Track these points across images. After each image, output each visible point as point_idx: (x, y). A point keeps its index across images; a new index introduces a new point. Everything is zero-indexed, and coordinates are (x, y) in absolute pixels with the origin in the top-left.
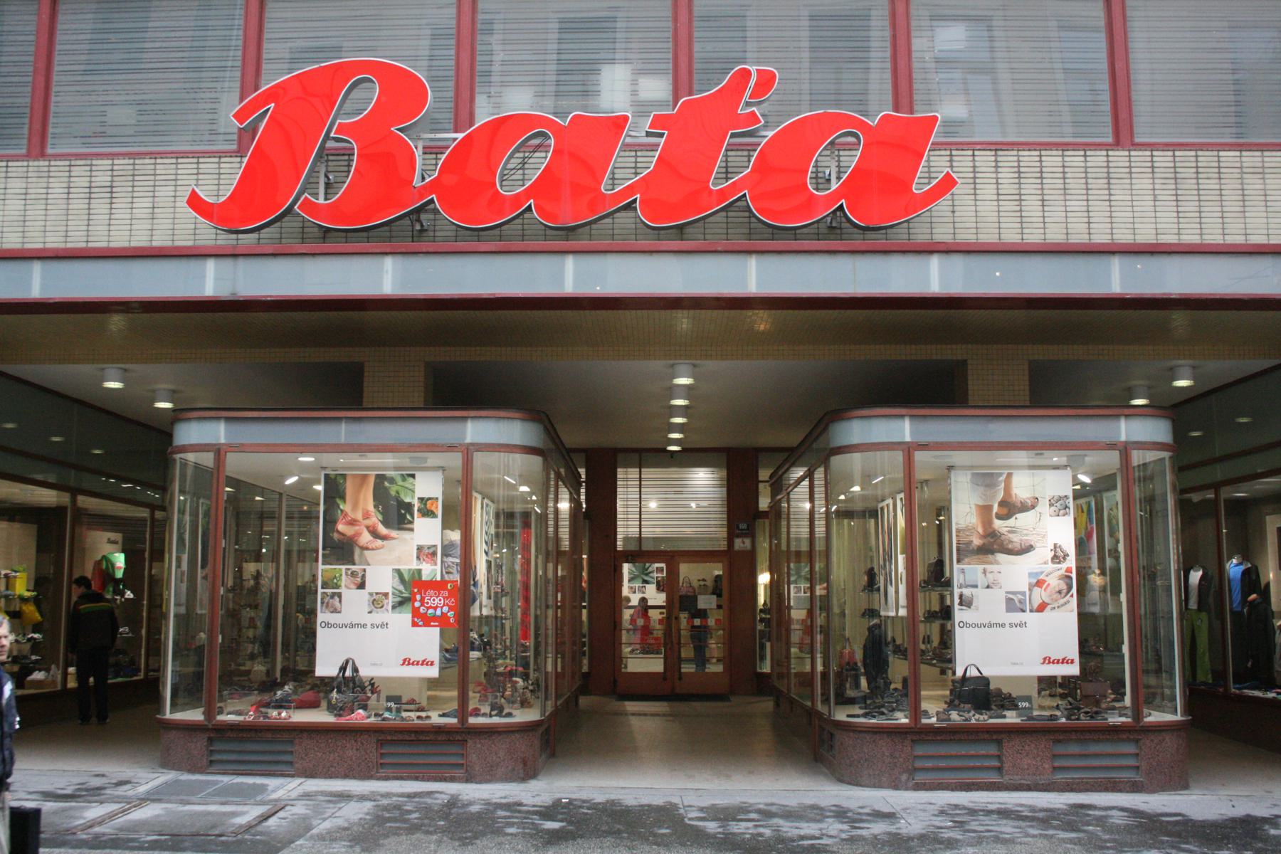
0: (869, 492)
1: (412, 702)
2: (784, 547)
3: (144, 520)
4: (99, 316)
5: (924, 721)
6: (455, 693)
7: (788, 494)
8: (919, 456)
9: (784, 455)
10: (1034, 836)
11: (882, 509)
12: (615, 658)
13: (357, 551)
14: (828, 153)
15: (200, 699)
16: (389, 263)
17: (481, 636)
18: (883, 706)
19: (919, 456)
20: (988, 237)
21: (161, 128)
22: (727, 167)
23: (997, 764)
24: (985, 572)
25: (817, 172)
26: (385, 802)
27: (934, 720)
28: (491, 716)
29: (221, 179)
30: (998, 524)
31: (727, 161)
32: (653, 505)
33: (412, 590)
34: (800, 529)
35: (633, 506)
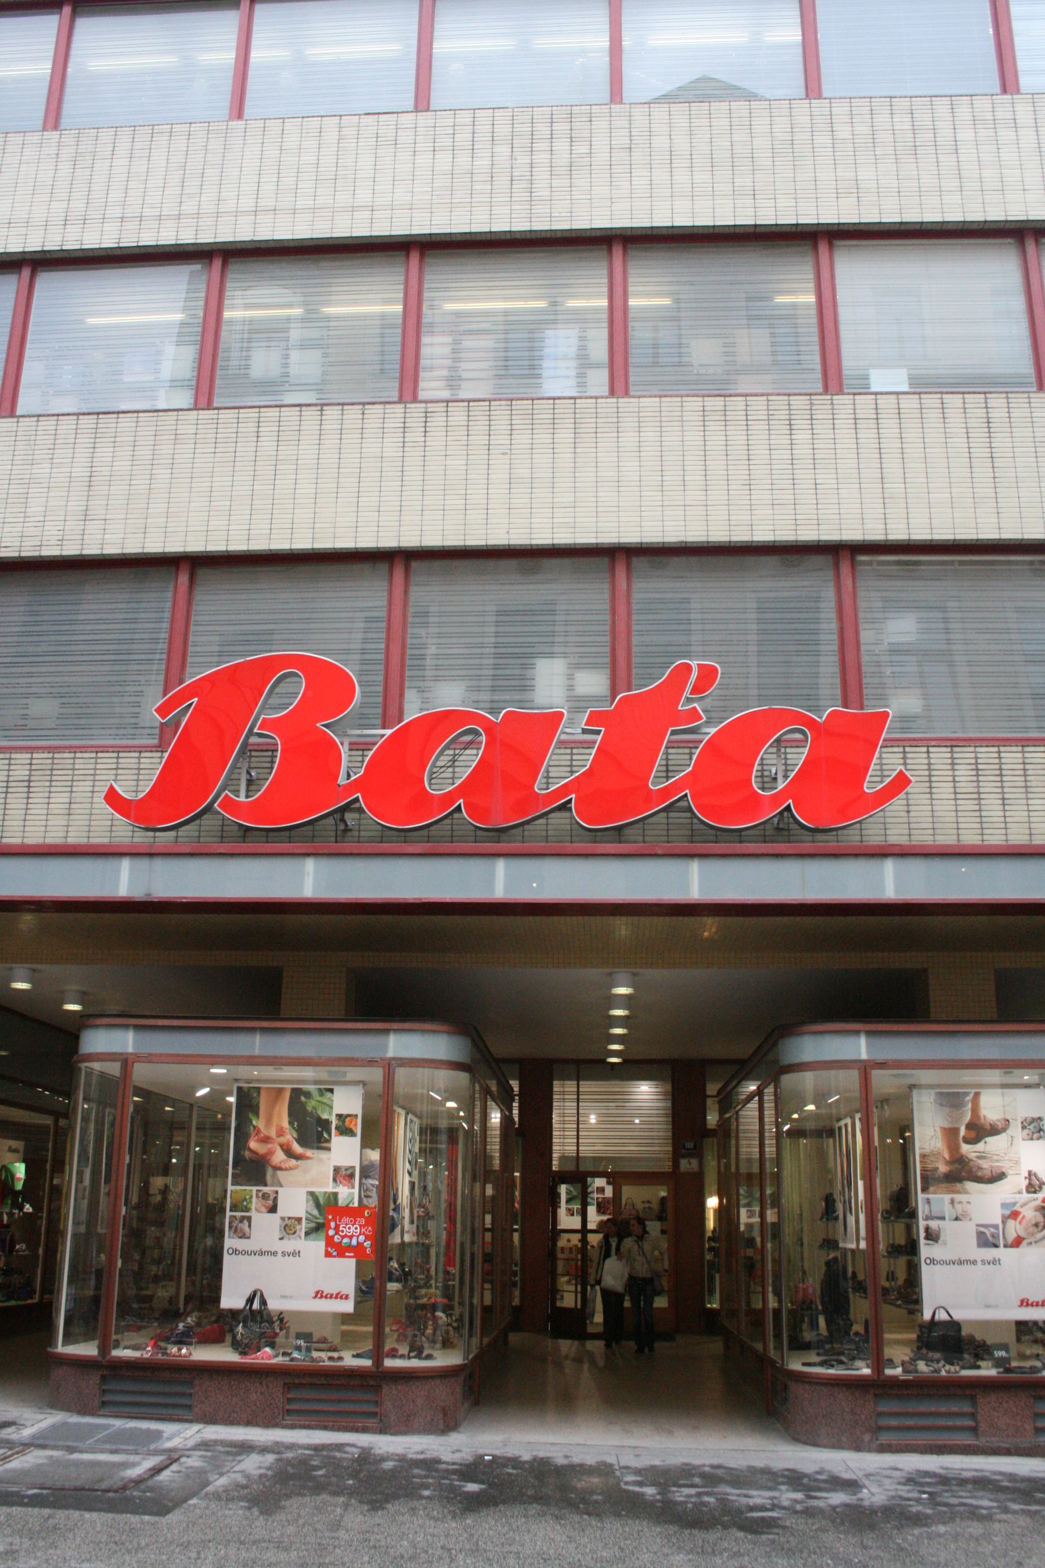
0: (823, 1111)
1: (324, 1340)
2: (733, 1169)
3: (48, 1127)
4: (10, 915)
5: (889, 1372)
6: (370, 1329)
8: (876, 1074)
10: (1015, 1512)
11: (840, 1128)
13: (269, 1172)
14: (774, 750)
15: (95, 1329)
16: (310, 865)
17: (402, 1265)
18: (842, 1354)
19: (876, 1074)
20: (946, 838)
21: (82, 721)
22: (667, 765)
23: (970, 1423)
24: (952, 1202)
25: (762, 770)
26: (290, 1455)
27: (899, 1371)
28: (409, 1358)
29: (139, 774)
30: (965, 1148)
31: (667, 759)
32: (593, 1119)
33: (326, 1213)
34: (749, 1149)
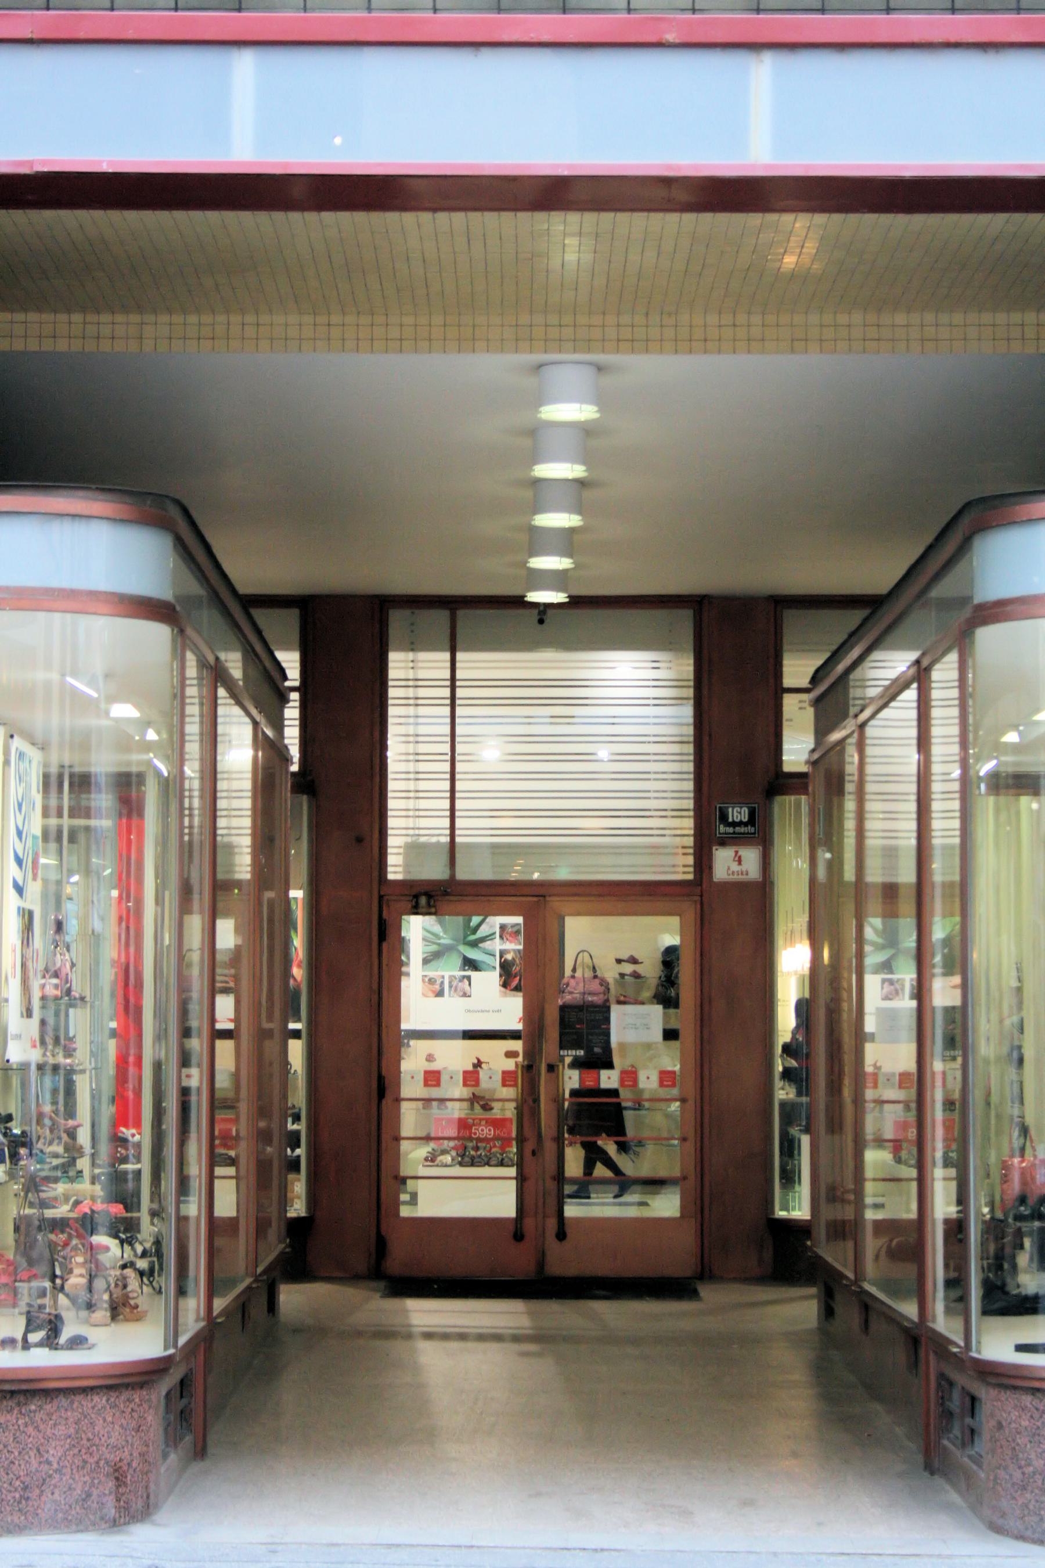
2: (849, 874)
7: (862, 726)
9: (855, 617)
12: (383, 1179)
28: (26, 1345)
35: (432, 757)
